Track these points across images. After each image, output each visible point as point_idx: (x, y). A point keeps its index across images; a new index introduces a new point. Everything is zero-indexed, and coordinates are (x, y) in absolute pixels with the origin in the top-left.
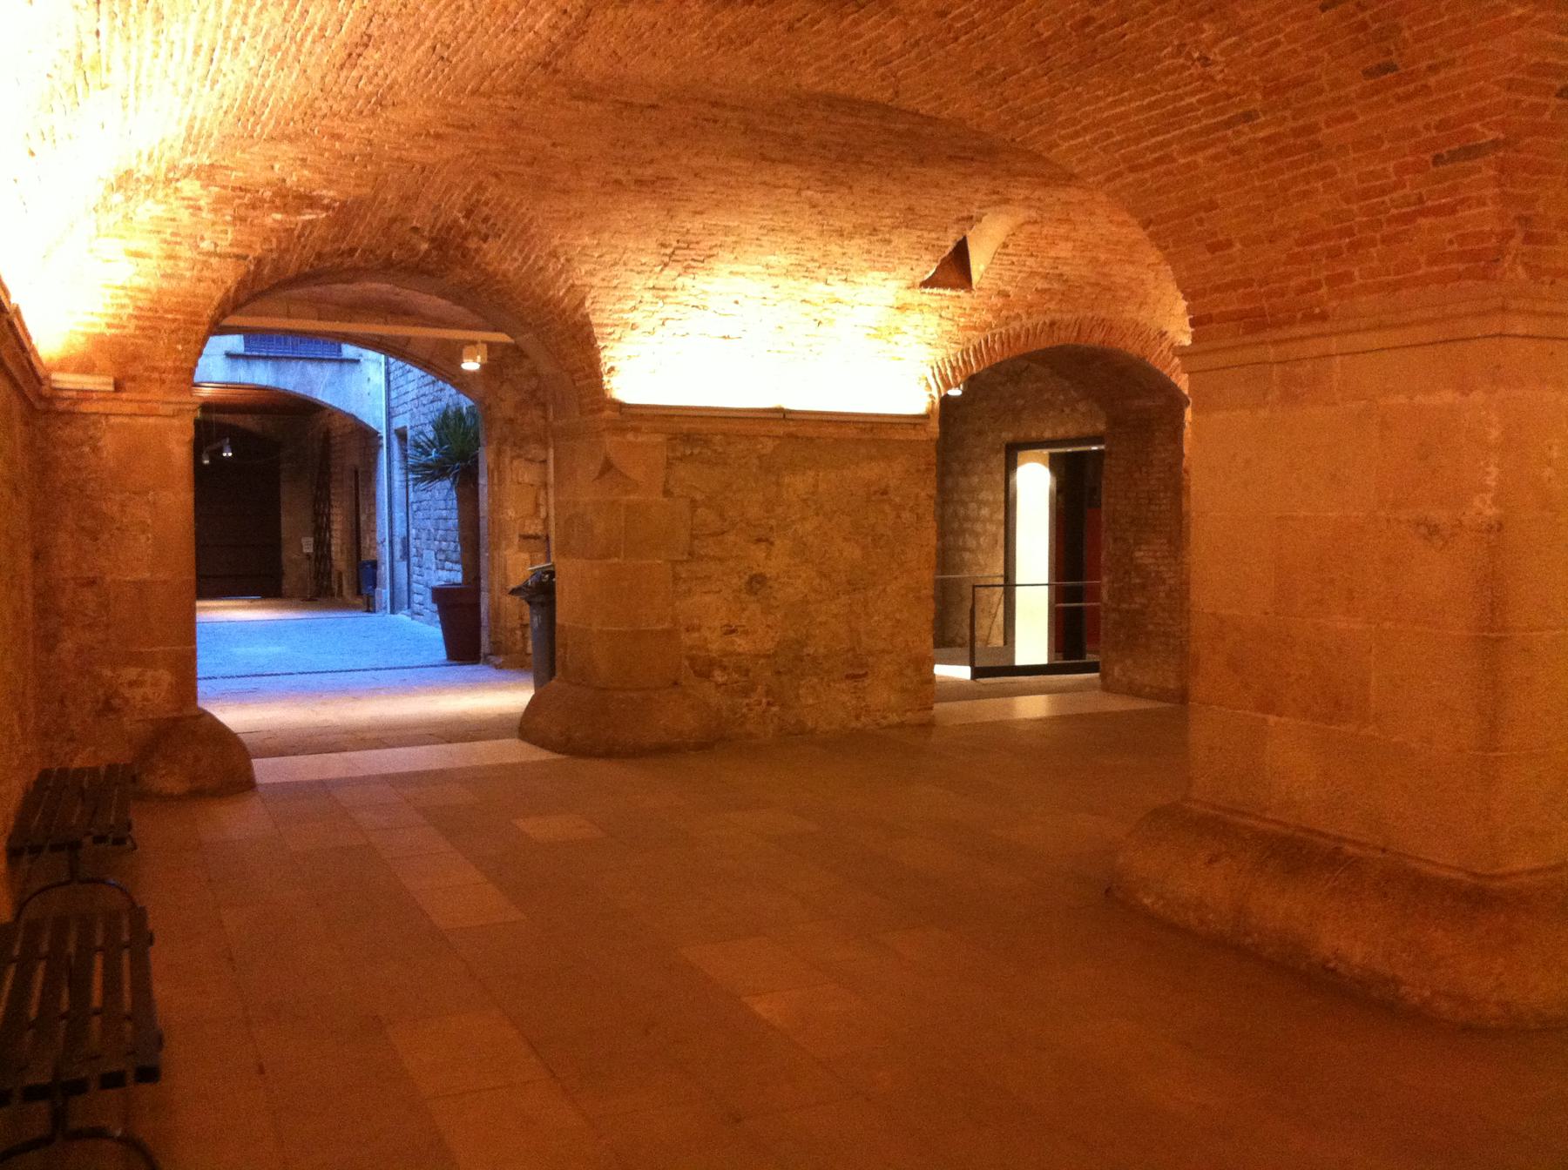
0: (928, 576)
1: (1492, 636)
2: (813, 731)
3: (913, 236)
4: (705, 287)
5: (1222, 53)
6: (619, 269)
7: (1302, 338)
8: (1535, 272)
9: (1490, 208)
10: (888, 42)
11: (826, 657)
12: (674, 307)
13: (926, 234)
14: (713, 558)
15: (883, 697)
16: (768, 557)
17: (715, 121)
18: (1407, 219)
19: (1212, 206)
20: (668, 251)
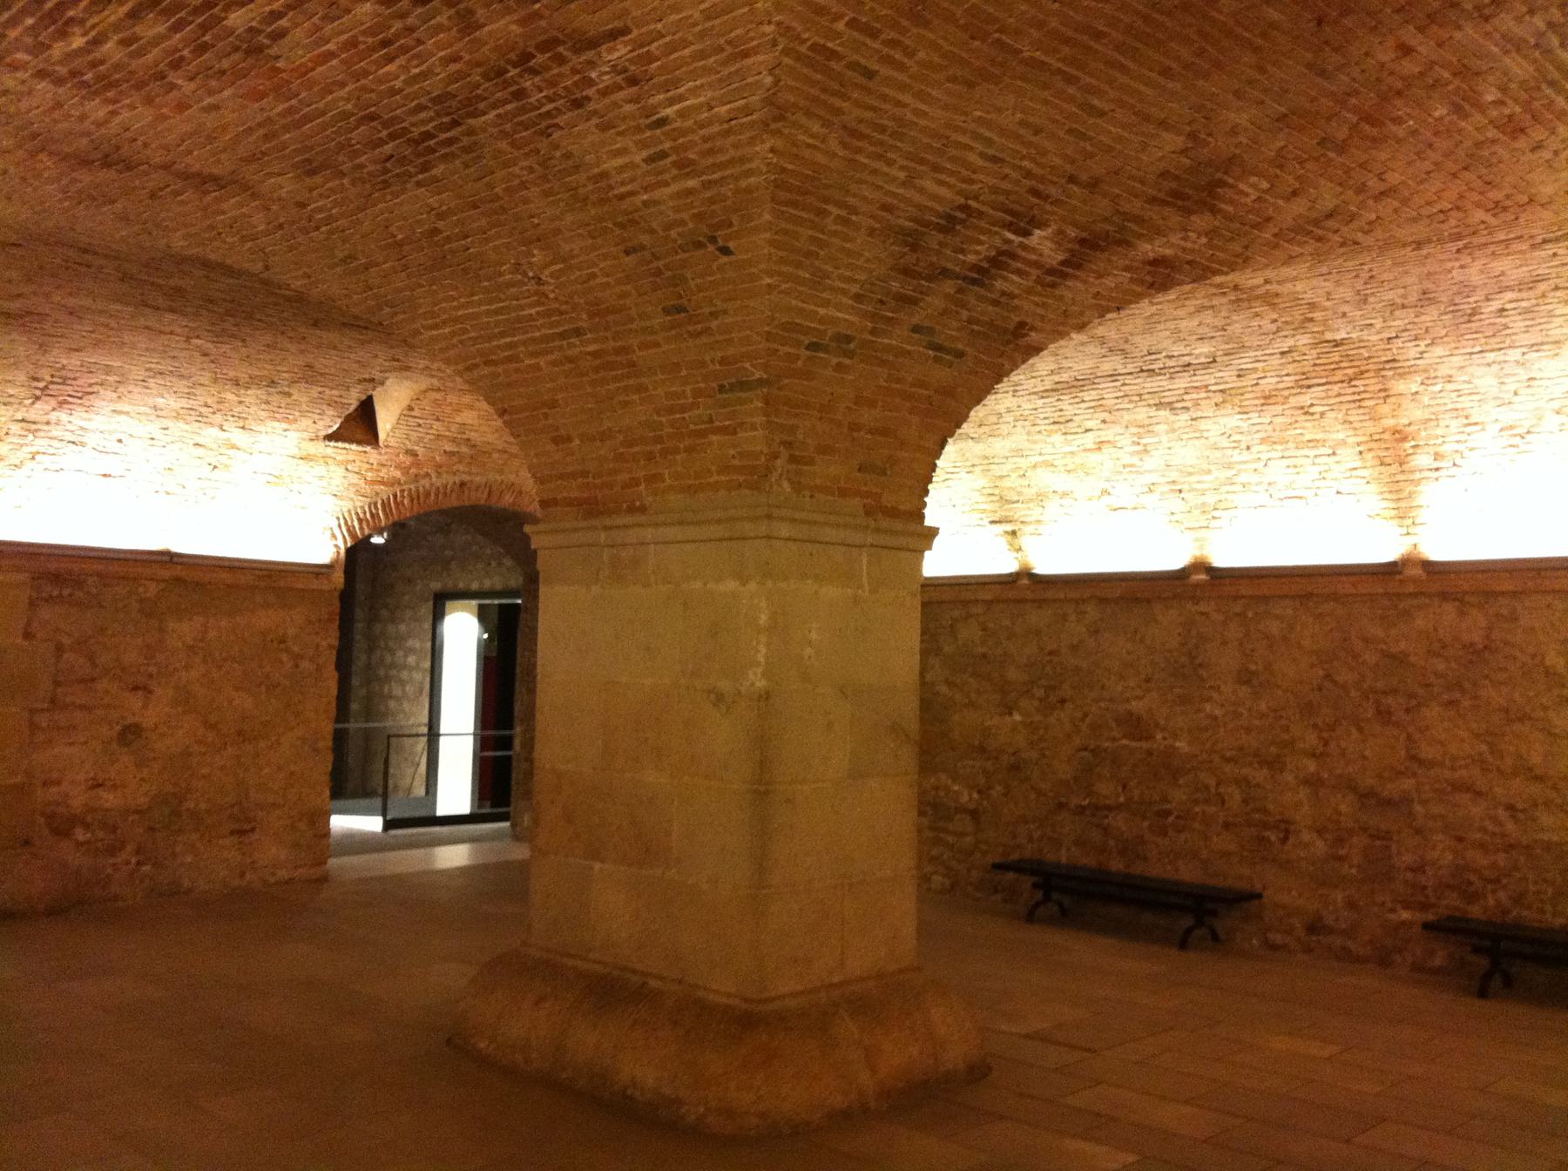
0: (328, 727)
1: (763, 791)
2: (190, 890)
3: (315, 391)
4: (85, 424)
5: (552, 275)
7: (626, 526)
8: (798, 487)
9: (760, 433)
10: (254, 220)
11: (208, 812)
12: (48, 442)
13: (327, 391)
14: (82, 707)
15: (273, 854)
16: (145, 706)
17: (89, 266)
18: (702, 434)
19: (553, 404)
20: (41, 385)
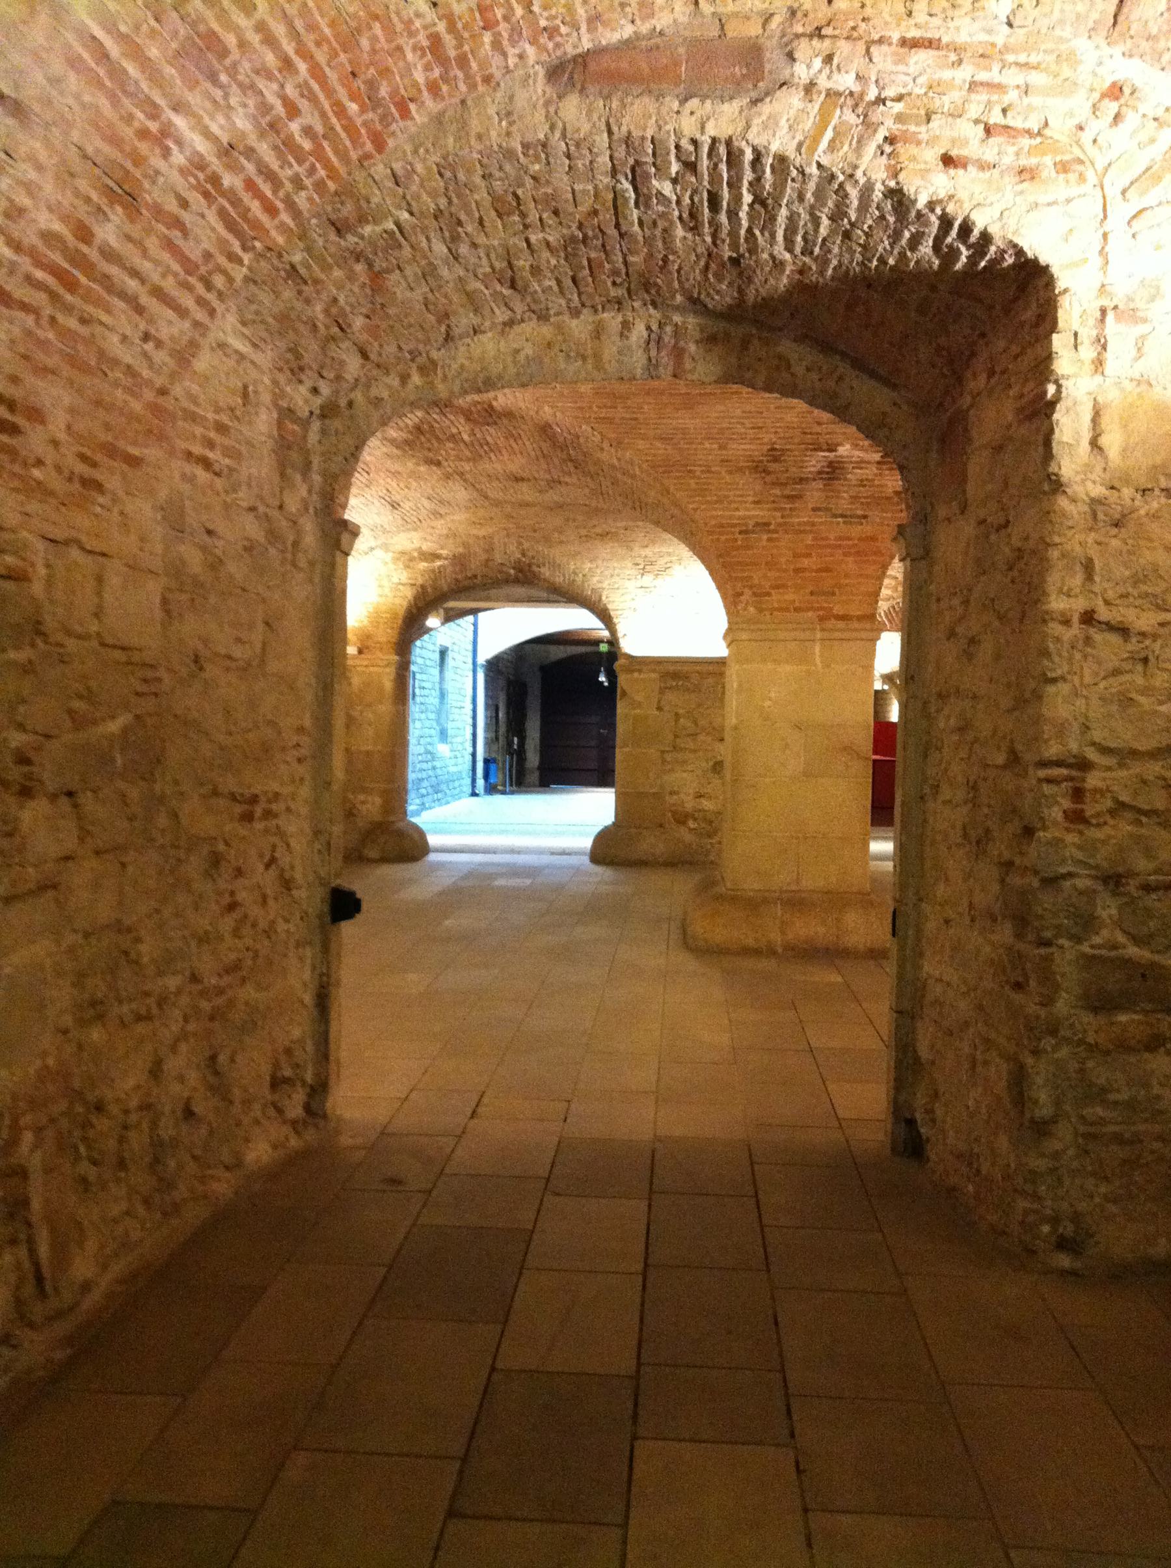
6: (616, 579)
